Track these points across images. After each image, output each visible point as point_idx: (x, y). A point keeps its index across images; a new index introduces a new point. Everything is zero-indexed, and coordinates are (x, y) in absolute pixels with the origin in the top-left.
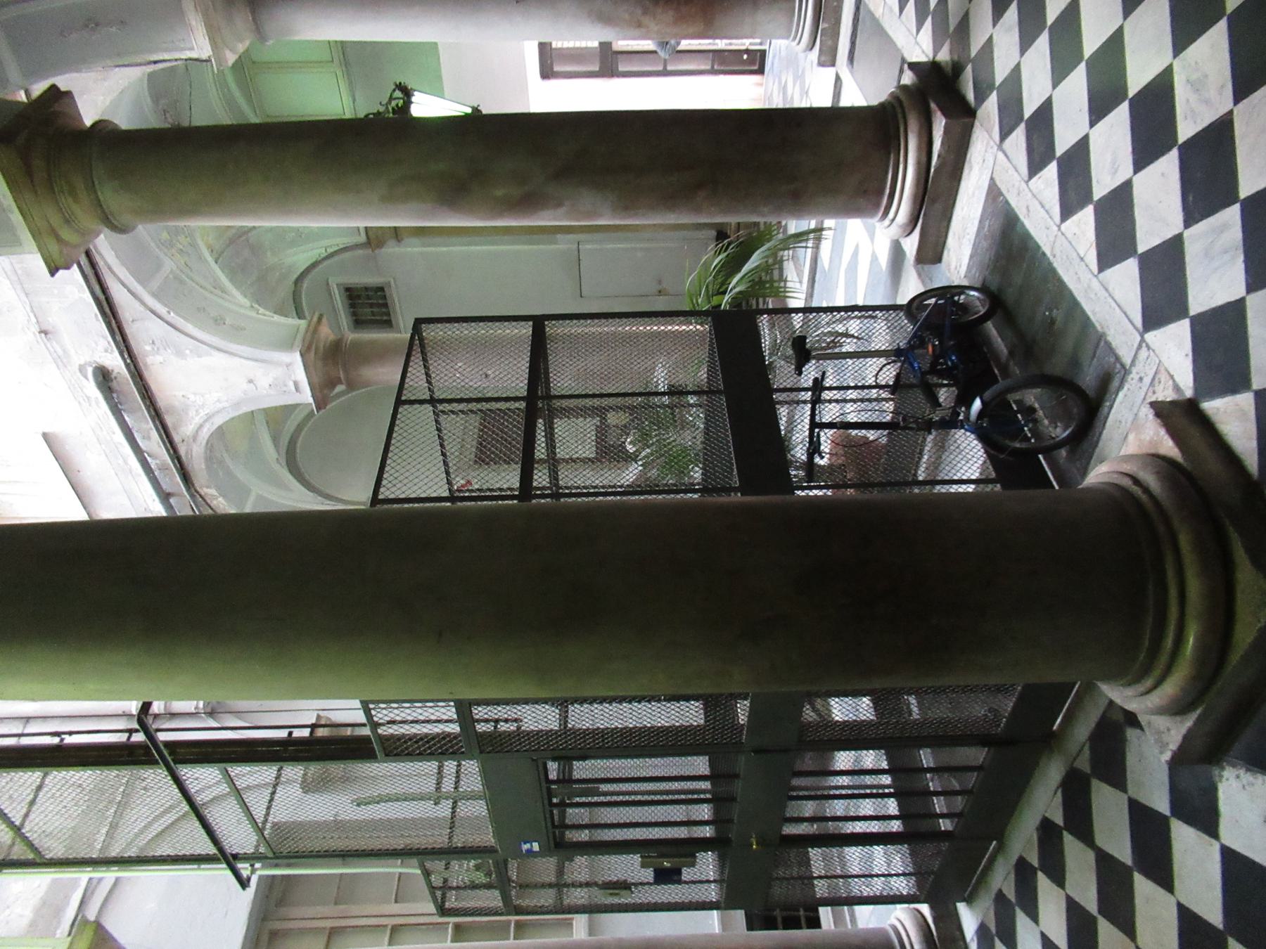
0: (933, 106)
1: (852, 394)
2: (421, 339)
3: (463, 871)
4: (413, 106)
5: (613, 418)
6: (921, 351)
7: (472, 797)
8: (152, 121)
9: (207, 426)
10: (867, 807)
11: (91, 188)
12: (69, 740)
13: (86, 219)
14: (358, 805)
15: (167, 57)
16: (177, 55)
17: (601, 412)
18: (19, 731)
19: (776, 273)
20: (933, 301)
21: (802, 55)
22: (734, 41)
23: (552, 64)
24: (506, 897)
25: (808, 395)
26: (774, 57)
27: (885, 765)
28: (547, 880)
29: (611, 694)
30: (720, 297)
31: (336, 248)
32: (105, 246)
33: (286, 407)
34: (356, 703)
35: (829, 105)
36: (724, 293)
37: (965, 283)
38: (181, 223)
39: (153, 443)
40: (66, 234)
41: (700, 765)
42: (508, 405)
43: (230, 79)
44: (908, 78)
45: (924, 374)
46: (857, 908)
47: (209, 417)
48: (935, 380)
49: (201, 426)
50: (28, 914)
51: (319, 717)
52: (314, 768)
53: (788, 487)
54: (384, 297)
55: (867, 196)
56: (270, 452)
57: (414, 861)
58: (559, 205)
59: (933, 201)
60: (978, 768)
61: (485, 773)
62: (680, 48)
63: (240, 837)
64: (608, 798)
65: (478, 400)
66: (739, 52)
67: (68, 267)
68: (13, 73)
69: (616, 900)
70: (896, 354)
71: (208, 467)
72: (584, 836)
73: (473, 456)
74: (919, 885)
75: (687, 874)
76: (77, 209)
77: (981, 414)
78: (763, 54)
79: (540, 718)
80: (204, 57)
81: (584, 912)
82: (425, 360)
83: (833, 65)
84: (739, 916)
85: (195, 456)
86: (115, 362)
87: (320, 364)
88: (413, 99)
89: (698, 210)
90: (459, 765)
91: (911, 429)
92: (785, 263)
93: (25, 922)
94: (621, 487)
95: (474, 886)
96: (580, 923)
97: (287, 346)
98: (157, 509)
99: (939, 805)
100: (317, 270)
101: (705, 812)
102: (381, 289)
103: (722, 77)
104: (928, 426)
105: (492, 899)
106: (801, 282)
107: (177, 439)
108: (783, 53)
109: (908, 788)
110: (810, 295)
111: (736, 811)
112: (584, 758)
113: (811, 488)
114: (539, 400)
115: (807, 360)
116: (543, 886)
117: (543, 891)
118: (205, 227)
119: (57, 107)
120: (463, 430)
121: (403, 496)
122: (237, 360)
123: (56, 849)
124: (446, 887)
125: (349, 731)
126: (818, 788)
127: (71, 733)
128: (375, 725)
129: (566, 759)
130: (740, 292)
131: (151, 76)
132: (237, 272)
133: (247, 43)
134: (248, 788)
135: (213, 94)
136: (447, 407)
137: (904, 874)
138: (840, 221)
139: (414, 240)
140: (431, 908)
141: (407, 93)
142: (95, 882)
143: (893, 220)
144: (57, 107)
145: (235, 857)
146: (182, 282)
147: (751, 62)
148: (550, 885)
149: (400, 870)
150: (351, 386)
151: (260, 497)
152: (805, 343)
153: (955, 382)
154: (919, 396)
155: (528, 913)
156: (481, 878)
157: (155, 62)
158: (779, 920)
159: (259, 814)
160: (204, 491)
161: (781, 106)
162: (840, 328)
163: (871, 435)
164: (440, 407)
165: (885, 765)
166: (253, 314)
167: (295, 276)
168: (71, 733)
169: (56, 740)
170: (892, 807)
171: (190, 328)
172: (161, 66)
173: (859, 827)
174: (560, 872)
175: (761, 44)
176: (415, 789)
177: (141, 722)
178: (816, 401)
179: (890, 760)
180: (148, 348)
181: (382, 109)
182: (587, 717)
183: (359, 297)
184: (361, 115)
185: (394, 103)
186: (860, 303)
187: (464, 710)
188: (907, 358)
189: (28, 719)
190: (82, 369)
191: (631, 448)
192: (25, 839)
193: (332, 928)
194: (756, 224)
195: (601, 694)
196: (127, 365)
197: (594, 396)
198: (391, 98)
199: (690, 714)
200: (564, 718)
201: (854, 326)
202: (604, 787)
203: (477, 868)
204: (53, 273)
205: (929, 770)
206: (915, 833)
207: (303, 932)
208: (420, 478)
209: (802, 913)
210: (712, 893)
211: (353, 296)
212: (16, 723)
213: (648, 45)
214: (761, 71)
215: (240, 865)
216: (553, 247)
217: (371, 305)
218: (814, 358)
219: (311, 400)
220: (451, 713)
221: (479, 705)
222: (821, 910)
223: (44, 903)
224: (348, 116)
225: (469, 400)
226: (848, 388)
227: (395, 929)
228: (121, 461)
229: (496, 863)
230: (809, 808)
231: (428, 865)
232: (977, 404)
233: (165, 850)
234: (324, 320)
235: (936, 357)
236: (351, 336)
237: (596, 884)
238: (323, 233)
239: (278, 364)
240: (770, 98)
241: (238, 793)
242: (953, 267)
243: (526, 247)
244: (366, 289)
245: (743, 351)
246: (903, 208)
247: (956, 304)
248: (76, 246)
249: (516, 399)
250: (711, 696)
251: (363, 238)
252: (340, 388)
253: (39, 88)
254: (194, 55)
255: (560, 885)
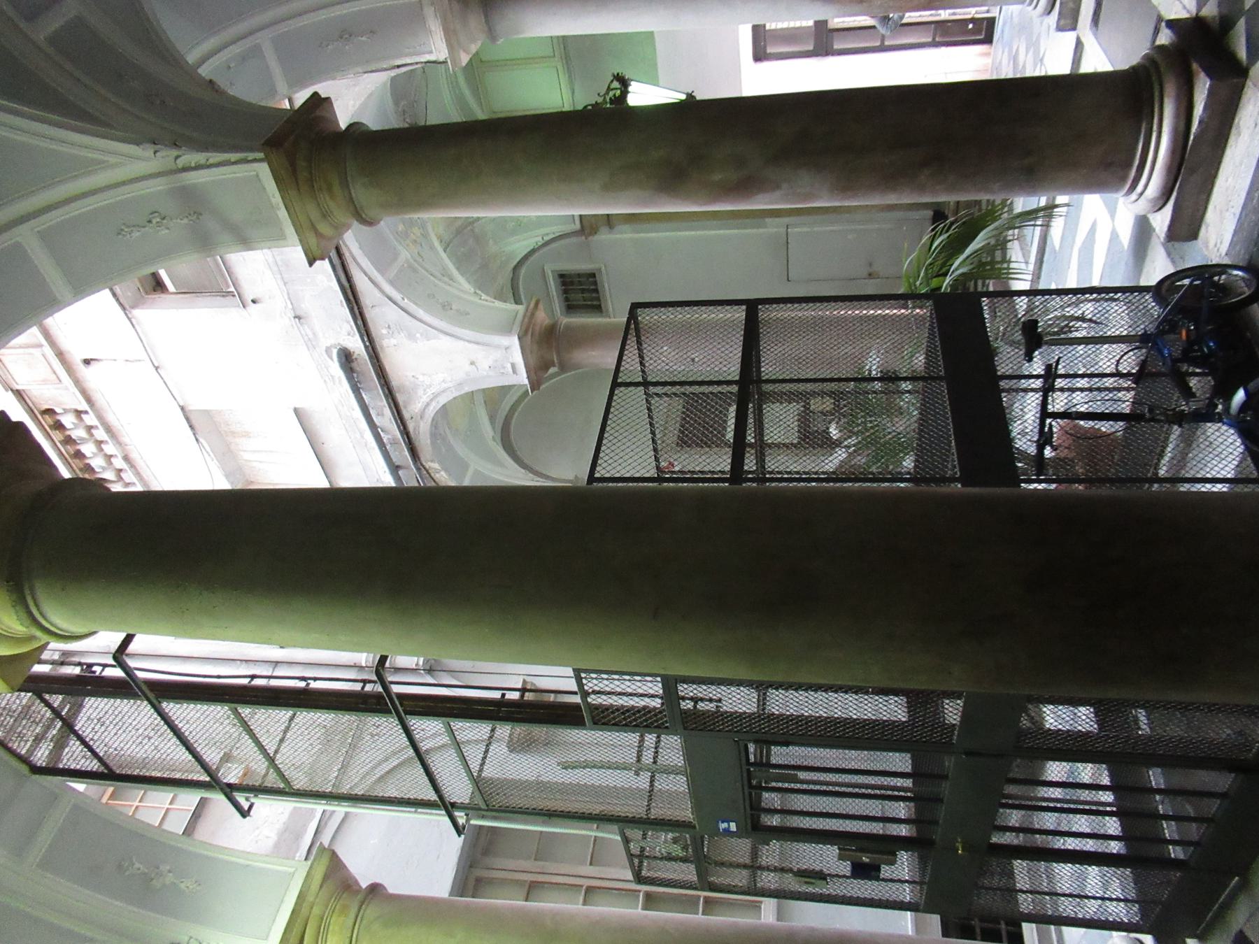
0: (1195, 66)
1: (1082, 383)
2: (637, 323)
3: (662, 842)
4: (629, 96)
5: (816, 404)
6: (1172, 337)
7: (668, 771)
8: (394, 123)
9: (434, 404)
10: (1082, 823)
11: (345, 184)
12: (314, 685)
13: (340, 215)
14: (565, 768)
15: (409, 61)
16: (417, 59)
17: (803, 397)
18: (269, 674)
19: (998, 254)
20: (1186, 282)
21: (1037, 21)
22: (958, 11)
23: (765, 47)
24: (702, 874)
25: (1038, 383)
26: (1004, 24)
27: (1106, 781)
28: (741, 861)
29: (822, 681)
30: (941, 278)
31: (552, 236)
32: (353, 241)
33: (503, 387)
34: (569, 671)
35: (1067, 71)
36: (945, 275)
37: (1226, 261)
38: (415, 216)
39: (385, 419)
40: (324, 228)
41: (900, 761)
42: (711, 389)
43: (461, 80)
44: (1165, 37)
45: (1175, 361)
46: (1065, 929)
47: (435, 396)
48: (1185, 368)
49: (428, 405)
50: (274, 837)
51: (524, 682)
52: (520, 729)
53: (1013, 478)
54: (595, 283)
55: (1111, 167)
56: (488, 431)
57: (615, 827)
58: (778, 187)
59: (1192, 171)
60: (1223, 796)
61: (689, 754)
62: (904, 21)
63: (459, 789)
64: (805, 786)
65: (682, 384)
66: (966, 21)
67: (323, 259)
68: (282, 86)
69: (810, 889)
70: (1144, 340)
71: (433, 443)
72: (775, 821)
73: (675, 438)
74: (1144, 913)
75: (886, 871)
76: (331, 204)
77: (1244, 407)
78: (991, 22)
79: (740, 701)
80: (441, 59)
81: (775, 897)
82: (639, 343)
83: (1074, 29)
84: (935, 920)
85: (422, 431)
86: (356, 344)
87: (535, 347)
88: (630, 89)
89: (922, 189)
90: (493, 730)
91: (1158, 421)
92: (1009, 245)
93: (270, 843)
94: (823, 473)
95: (670, 858)
96: (769, 908)
97: (505, 330)
98: (388, 481)
99: (1169, 830)
100: (532, 259)
101: (901, 810)
102: (593, 275)
103: (943, 49)
104: (1179, 418)
105: (688, 872)
106: (1027, 263)
107: (406, 415)
108: (1016, 20)
109: (1132, 807)
110: (1037, 275)
111: (942, 813)
112: (787, 744)
113: (1040, 482)
114: (750, 387)
115: (1039, 346)
116: (738, 866)
117: (737, 871)
118: (436, 219)
119: (318, 113)
120: (669, 410)
121: (618, 475)
122: (461, 344)
123: (300, 782)
124: (641, 856)
125: (552, 697)
126: (1031, 799)
127: (315, 679)
128: (585, 694)
129: (766, 742)
130: (963, 274)
131: (393, 79)
132: (462, 262)
133: (479, 43)
134: (468, 742)
135: (447, 96)
136: (659, 390)
137: (1126, 900)
138: (1075, 196)
139: (626, 227)
140: (629, 876)
141: (624, 83)
142: (327, 815)
143: (1141, 194)
144: (318, 113)
145: (453, 805)
146: (415, 271)
147: (976, 31)
148: (745, 866)
149: (593, 834)
150: (563, 368)
151: (477, 472)
152: (1037, 328)
153: (1211, 370)
154: (1167, 385)
155: (721, 891)
156: (677, 850)
157: (398, 67)
158: (978, 931)
159: (475, 767)
160: (428, 465)
161: (1010, 76)
162: (1071, 311)
163: (1104, 427)
164: (652, 389)
165: (1106, 781)
166: (476, 300)
167: (512, 266)
168: (315, 679)
169: (302, 684)
170: (1112, 826)
171: (420, 313)
172: (403, 70)
173: (1071, 844)
174: (755, 854)
175: (988, 12)
176: (618, 758)
177: (378, 674)
178: (1048, 390)
179: (1111, 775)
180: (384, 331)
181: (600, 100)
182: (785, 703)
183: (572, 283)
184: (580, 107)
185: (611, 94)
186: (1096, 283)
187: (670, 684)
188: (1155, 344)
189: (277, 663)
190: (328, 350)
191: (834, 432)
192: (278, 770)
193: (532, 882)
194: (978, 203)
195: (807, 681)
196: (366, 347)
197: (791, 381)
198: (609, 89)
199: (893, 709)
200: (762, 702)
201: (1088, 309)
202: (802, 775)
203: (675, 841)
204: (311, 264)
205: (1159, 791)
206: (1140, 855)
207: (503, 882)
208: (631, 460)
209: (1003, 926)
210: (906, 893)
211: (567, 281)
212: (267, 665)
213: (864, 20)
214: (988, 40)
215: (457, 814)
216: (761, 230)
217: (583, 291)
218: (1047, 343)
219: (526, 382)
220: (658, 688)
221: (684, 682)
222: (1024, 925)
223: (286, 829)
224: (567, 108)
225: (673, 384)
226: (1075, 376)
227: (590, 890)
228: (358, 436)
229: (697, 844)
230: (1015, 818)
231: (629, 832)
232: (1240, 395)
233: (392, 792)
234: (541, 306)
235: (1190, 342)
236: (566, 320)
237: (791, 870)
238: (540, 222)
239: (498, 347)
240: (998, 69)
241: (458, 745)
242: (1211, 245)
243: (754, 231)
244: (579, 275)
245: (966, 337)
246: (1154, 182)
247: (1216, 285)
248: (330, 239)
249: (729, 383)
250: (922, 692)
251: (578, 226)
252: (552, 370)
253: (301, 97)
254: (432, 58)
255: (754, 867)
